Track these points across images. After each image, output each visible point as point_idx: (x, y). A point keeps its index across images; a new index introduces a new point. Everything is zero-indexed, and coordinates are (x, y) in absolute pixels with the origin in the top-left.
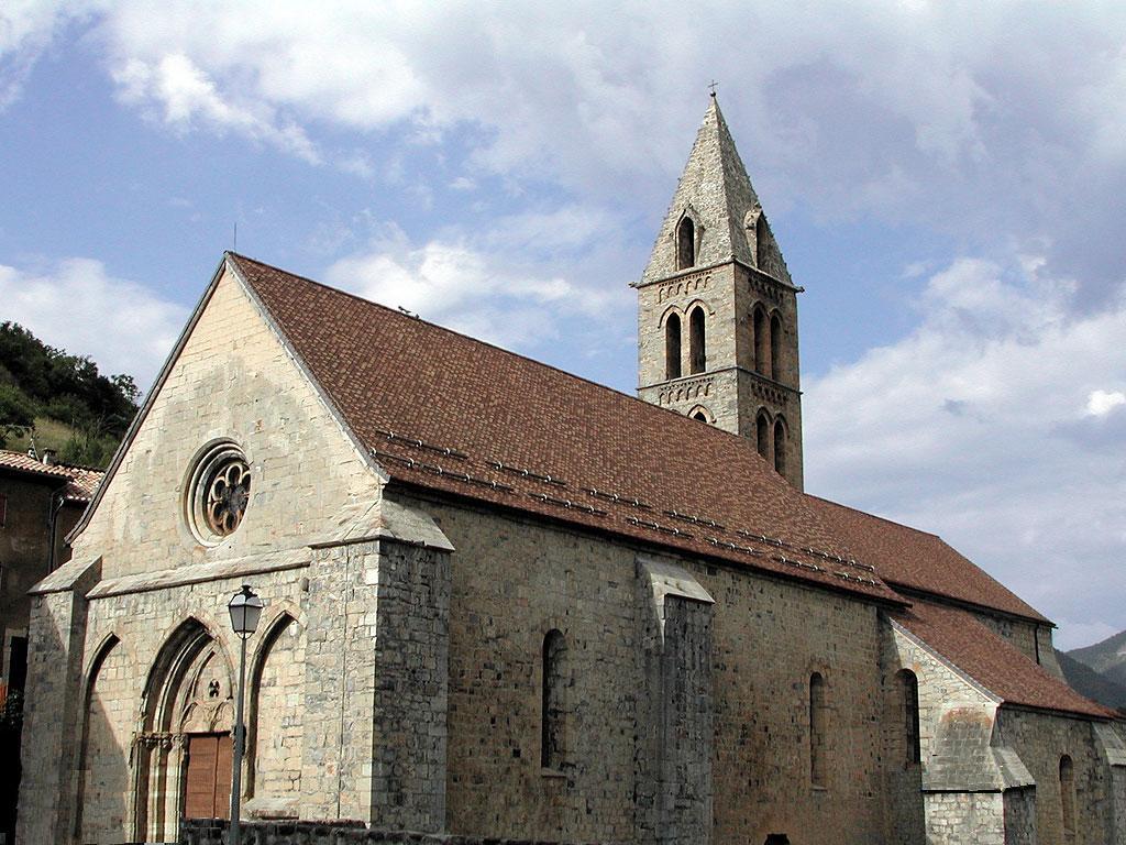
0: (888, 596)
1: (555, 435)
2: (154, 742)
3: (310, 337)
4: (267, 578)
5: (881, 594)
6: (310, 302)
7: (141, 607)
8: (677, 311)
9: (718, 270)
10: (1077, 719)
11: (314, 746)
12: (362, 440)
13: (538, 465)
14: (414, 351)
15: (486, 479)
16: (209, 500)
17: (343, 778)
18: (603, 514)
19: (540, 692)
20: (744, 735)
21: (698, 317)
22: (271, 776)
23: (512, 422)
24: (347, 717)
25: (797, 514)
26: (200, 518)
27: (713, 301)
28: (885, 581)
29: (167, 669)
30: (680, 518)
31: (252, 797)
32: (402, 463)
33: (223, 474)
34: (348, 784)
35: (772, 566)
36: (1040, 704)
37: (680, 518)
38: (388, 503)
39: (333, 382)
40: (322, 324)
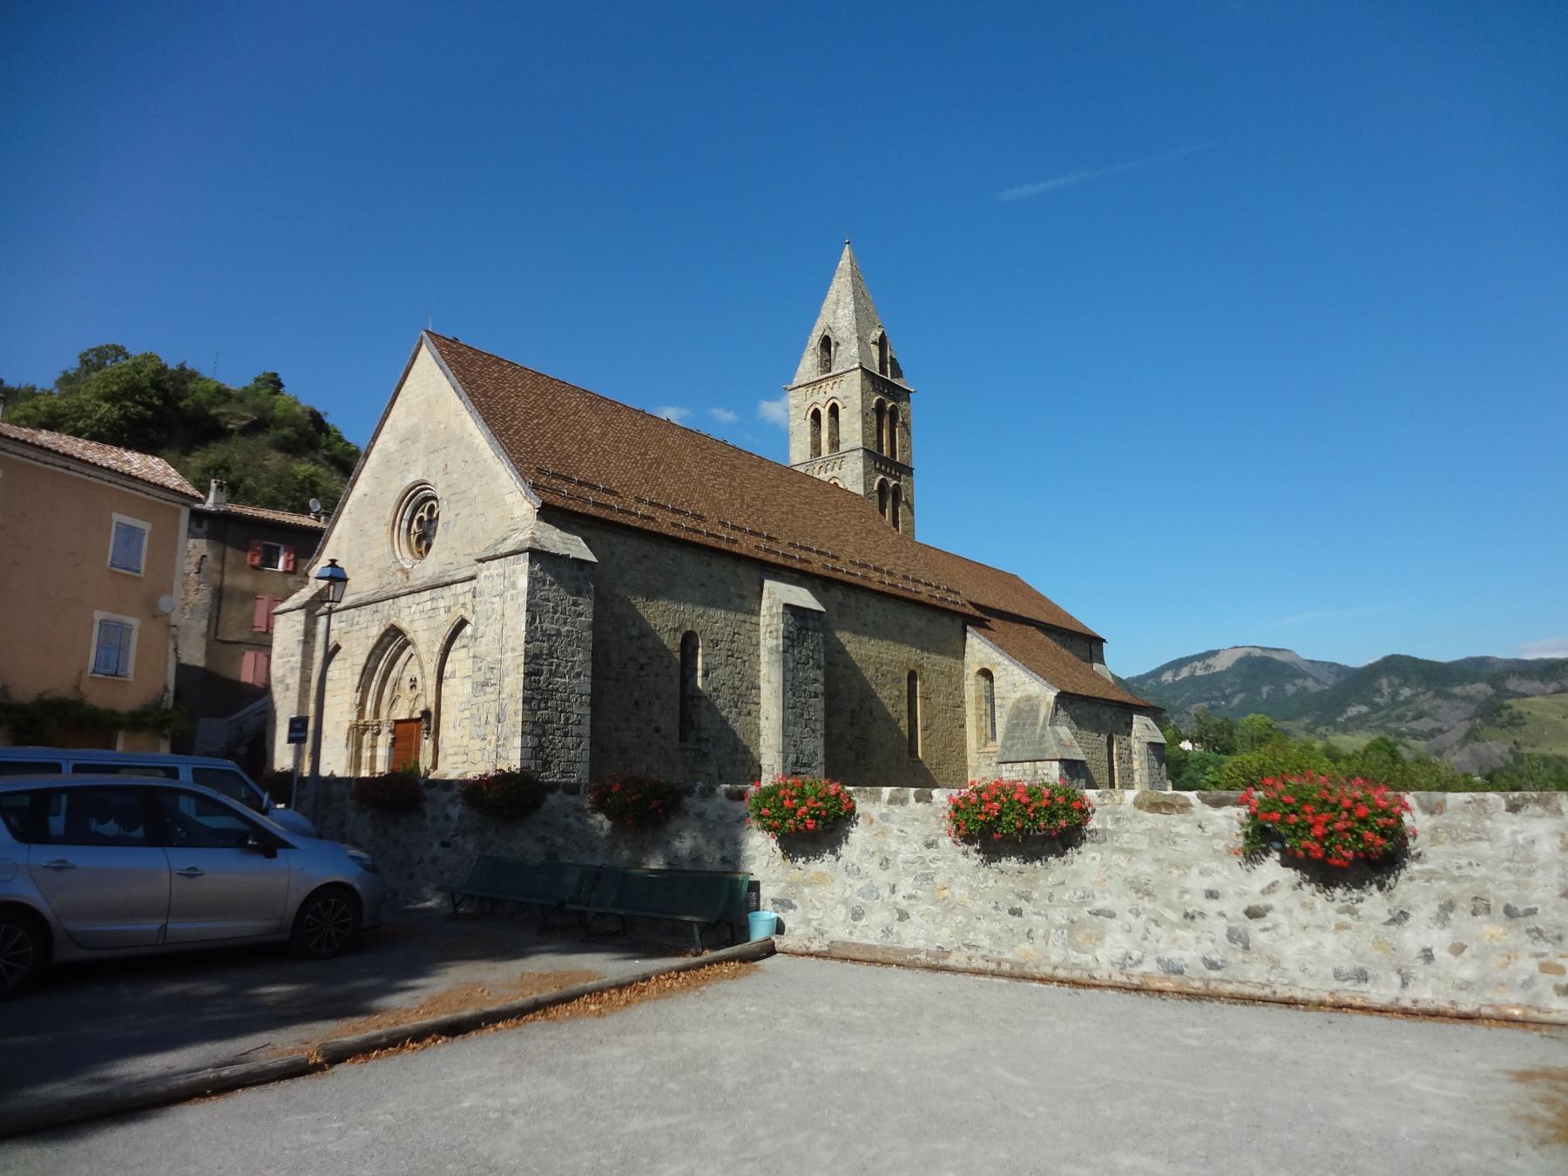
0: (971, 613)
1: (701, 483)
2: (366, 728)
3: (489, 397)
4: (448, 590)
5: (966, 611)
6: (496, 372)
7: (356, 619)
8: (818, 407)
9: (849, 374)
10: (1120, 707)
12: (523, 474)
13: (682, 503)
14: (584, 415)
15: (633, 509)
16: (412, 532)
17: (499, 750)
18: (735, 541)
19: (677, 680)
20: (853, 718)
21: (834, 410)
22: (451, 751)
23: (664, 471)
24: (503, 699)
25: (901, 552)
26: (404, 547)
27: (845, 398)
28: (971, 603)
30: (802, 548)
31: (436, 769)
32: (557, 492)
33: (423, 511)
34: (504, 754)
35: (877, 586)
36: (1090, 694)
37: (802, 548)
38: (542, 523)
39: (504, 430)
40: (503, 389)
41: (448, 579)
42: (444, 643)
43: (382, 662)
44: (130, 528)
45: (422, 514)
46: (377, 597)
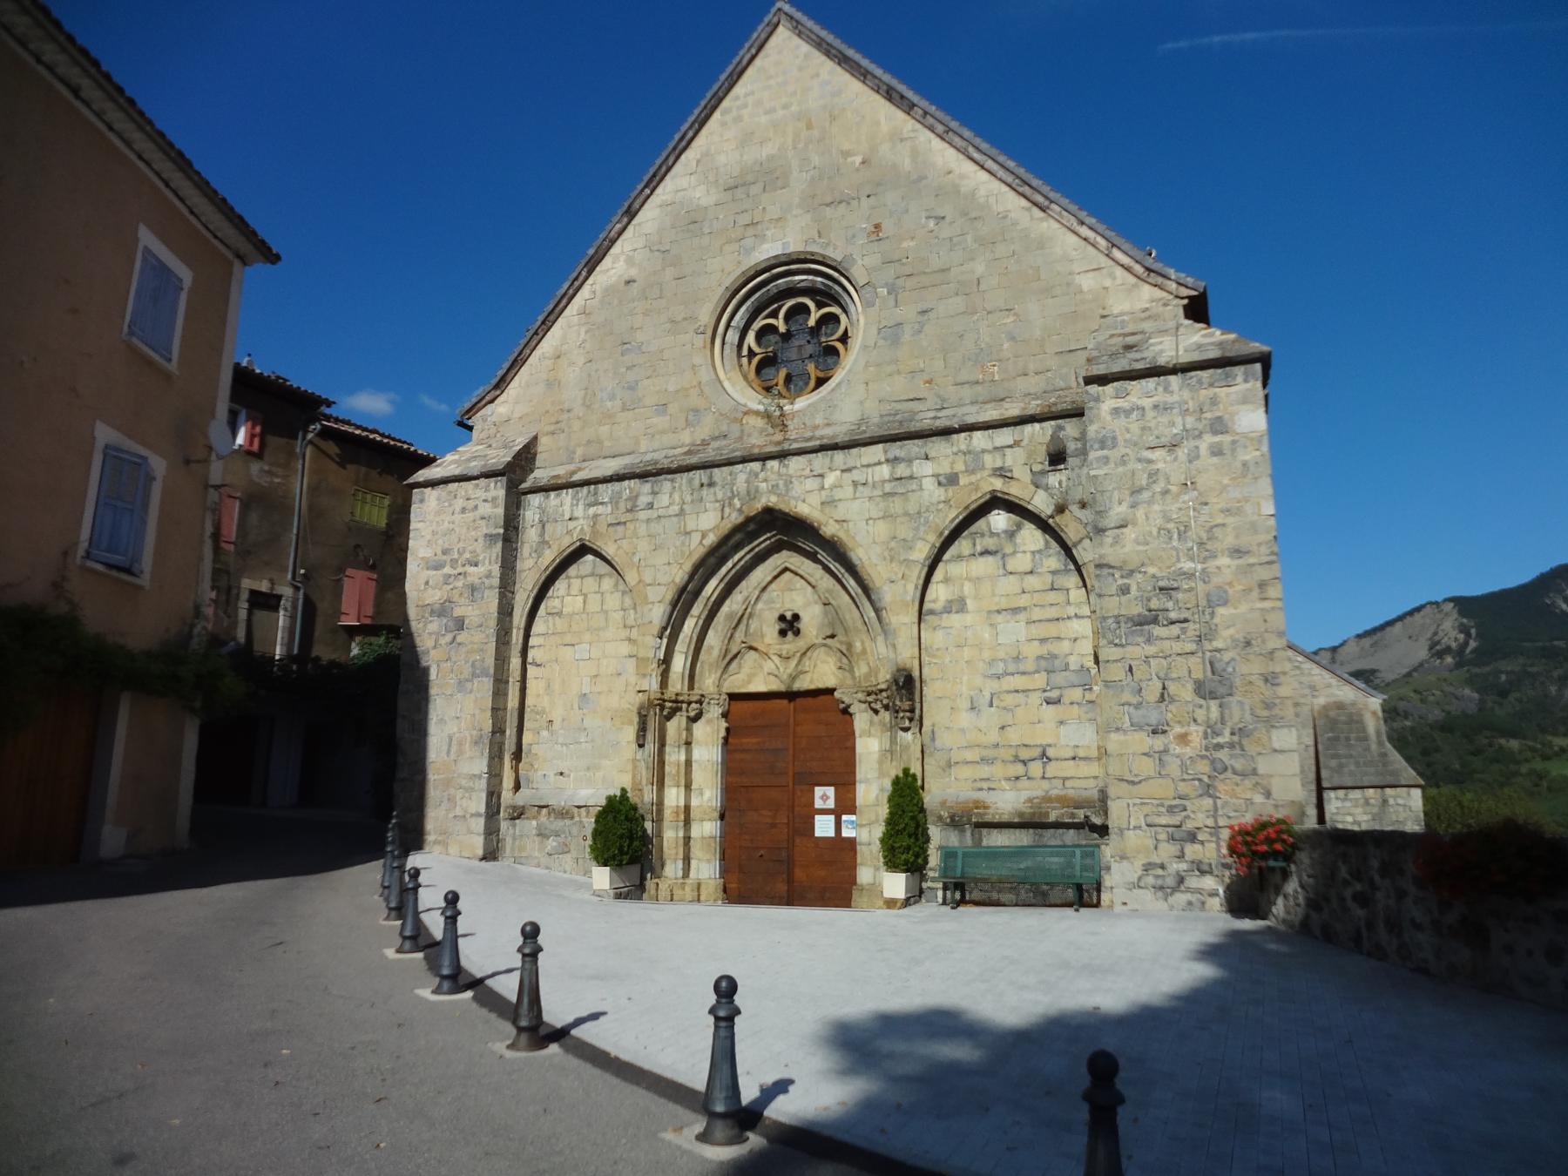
11: (1134, 700)
16: (745, 352)
29: (697, 593)
41: (926, 421)
42: (938, 545)
43: (713, 583)
44: (162, 270)
45: (811, 305)
46: (709, 454)
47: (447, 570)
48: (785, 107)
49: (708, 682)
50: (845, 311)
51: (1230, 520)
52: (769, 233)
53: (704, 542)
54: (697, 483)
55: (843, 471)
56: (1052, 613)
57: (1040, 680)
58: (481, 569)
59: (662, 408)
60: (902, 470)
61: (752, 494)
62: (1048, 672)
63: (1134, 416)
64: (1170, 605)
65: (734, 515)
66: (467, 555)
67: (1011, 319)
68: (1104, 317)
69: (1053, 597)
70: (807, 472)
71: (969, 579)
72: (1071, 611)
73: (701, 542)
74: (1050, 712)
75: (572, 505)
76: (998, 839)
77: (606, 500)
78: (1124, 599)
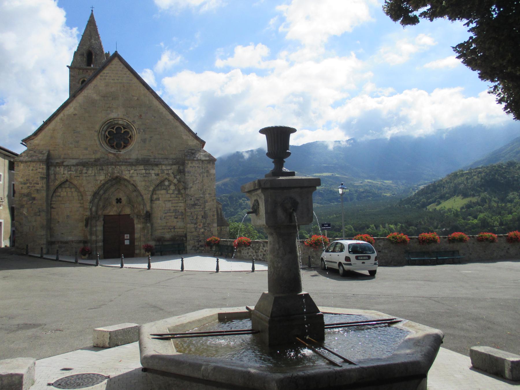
11: (192, 219)
47: (28, 185)
48: (118, 80)
49: (100, 213)
50: (131, 131)
51: (209, 188)
52: (114, 111)
53: (101, 183)
54: (98, 169)
55: (135, 170)
56: (176, 201)
57: (174, 214)
58: (40, 185)
59: (86, 149)
60: (147, 172)
61: (113, 173)
62: (175, 212)
63: (194, 168)
64: (198, 202)
65: (109, 177)
66: (35, 182)
67: (169, 142)
68: (187, 145)
69: (177, 199)
70: (126, 169)
71: (161, 194)
72: (180, 201)
73: (100, 183)
74: (175, 220)
75: (63, 170)
76: (167, 243)
77: (74, 170)
78: (191, 201)
